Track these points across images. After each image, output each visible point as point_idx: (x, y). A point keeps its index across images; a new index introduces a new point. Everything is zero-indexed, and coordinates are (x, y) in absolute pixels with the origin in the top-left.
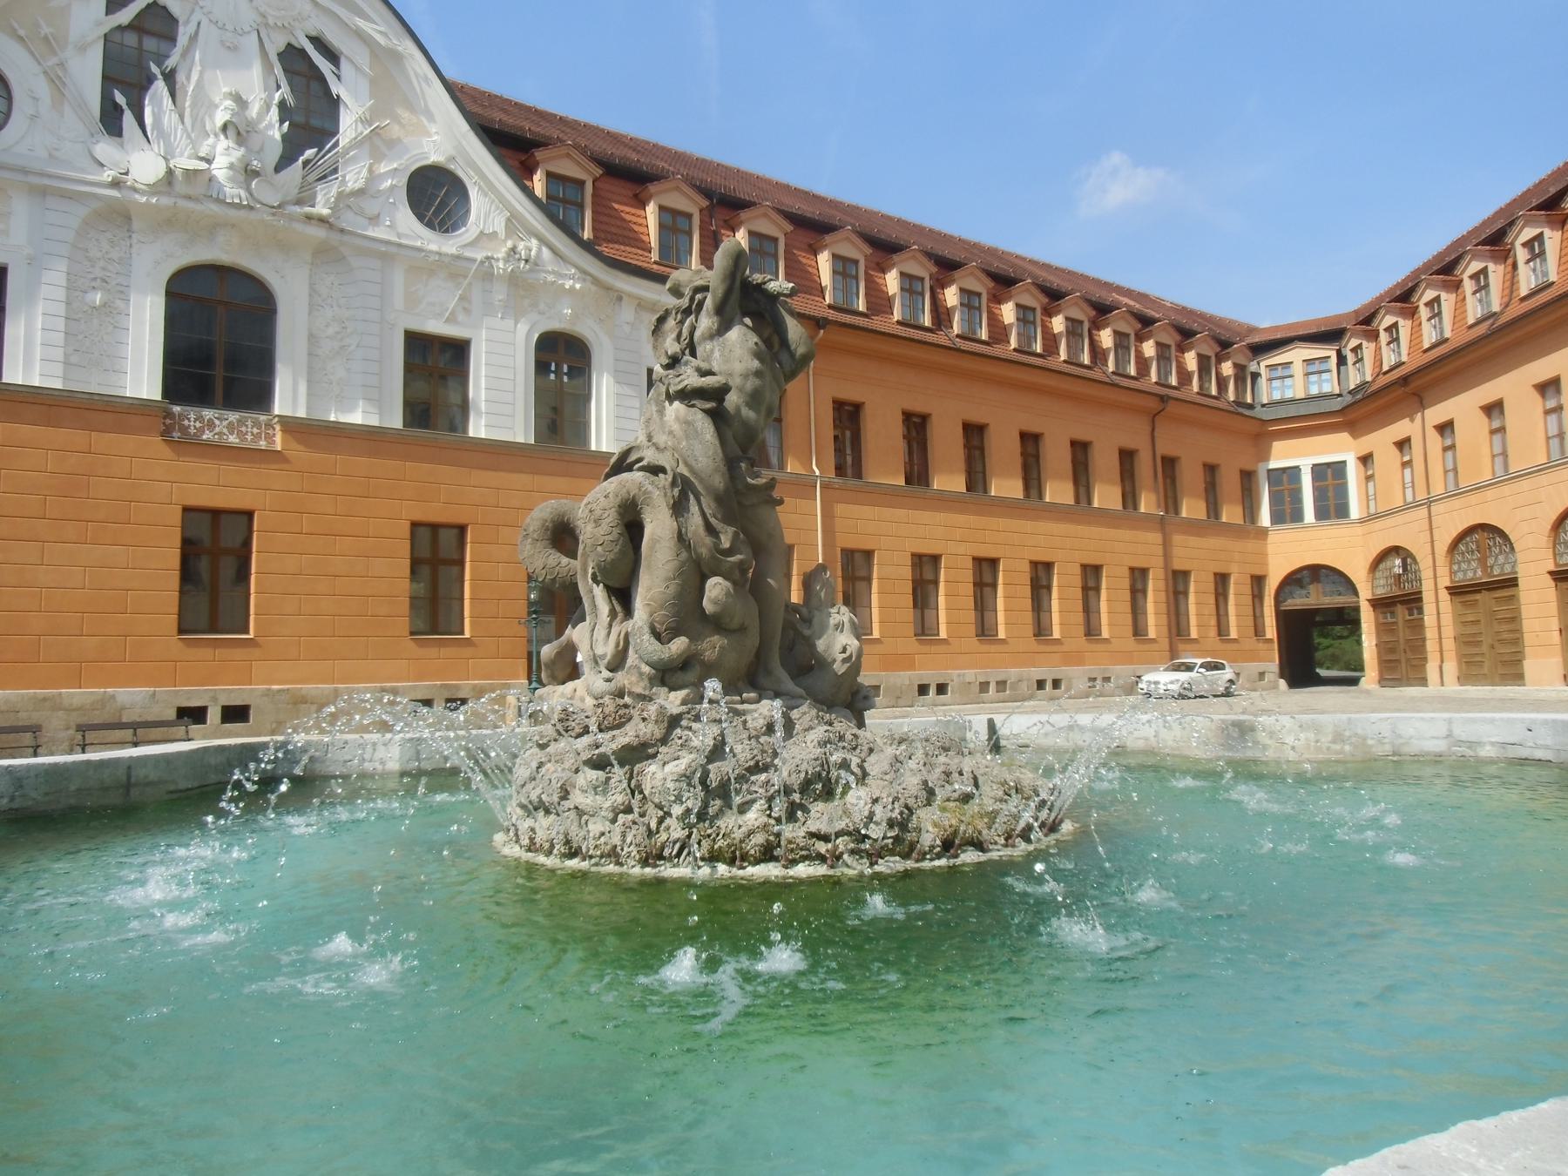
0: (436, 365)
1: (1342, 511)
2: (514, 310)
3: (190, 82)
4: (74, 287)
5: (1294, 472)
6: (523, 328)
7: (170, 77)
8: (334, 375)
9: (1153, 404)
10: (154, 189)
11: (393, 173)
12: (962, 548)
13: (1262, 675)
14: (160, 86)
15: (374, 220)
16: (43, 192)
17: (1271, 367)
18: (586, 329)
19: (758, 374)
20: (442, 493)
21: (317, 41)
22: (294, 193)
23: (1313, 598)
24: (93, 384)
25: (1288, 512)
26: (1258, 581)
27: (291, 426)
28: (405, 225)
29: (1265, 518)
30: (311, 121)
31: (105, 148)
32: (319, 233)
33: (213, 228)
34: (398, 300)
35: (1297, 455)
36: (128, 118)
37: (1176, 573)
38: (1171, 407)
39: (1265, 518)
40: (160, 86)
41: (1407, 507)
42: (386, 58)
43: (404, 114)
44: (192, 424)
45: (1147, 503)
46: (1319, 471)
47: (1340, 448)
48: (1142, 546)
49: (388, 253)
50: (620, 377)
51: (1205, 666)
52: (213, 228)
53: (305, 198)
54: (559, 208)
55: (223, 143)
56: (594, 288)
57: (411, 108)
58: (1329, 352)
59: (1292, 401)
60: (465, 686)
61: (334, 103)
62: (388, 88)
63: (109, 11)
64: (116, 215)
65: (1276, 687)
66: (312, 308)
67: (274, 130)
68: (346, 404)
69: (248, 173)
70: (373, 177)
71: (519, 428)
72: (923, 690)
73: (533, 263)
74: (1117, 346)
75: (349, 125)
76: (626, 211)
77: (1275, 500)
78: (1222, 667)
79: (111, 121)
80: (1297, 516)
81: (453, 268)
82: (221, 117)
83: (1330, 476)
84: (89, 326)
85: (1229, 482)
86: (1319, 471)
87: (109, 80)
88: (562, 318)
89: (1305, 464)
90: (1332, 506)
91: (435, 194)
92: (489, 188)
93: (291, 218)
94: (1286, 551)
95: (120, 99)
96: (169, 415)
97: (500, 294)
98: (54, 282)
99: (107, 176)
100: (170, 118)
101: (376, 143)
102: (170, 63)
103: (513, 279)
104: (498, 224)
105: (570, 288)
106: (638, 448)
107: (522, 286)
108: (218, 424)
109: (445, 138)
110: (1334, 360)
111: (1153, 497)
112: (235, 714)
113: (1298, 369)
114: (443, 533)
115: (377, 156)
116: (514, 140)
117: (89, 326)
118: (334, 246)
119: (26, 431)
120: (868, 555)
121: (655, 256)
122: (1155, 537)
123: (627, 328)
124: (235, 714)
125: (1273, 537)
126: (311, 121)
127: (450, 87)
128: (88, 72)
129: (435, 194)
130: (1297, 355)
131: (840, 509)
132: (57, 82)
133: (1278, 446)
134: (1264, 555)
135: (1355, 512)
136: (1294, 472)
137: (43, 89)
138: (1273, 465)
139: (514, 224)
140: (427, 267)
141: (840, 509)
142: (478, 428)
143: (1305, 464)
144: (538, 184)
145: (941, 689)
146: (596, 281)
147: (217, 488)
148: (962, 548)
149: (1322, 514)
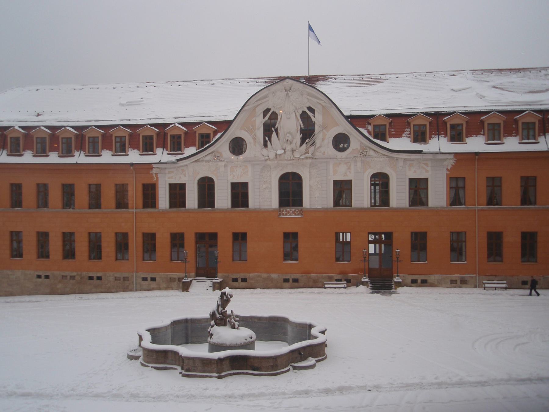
0: (342, 189)
7: (276, 130)
14: (274, 134)
18: (387, 170)
19: (209, 332)
21: (310, 109)
22: (304, 151)
32: (309, 161)
34: (331, 173)
36: (269, 142)
40: (274, 134)
41: (178, 253)
56: (387, 159)
61: (314, 124)
63: (264, 118)
79: (265, 145)
87: (265, 135)
93: (303, 159)
95: (267, 138)
96: (280, 211)
102: (276, 126)
106: (141, 362)
108: (291, 213)
112: (39, 277)
114: (91, 186)
123: (401, 168)
124: (39, 277)
128: (260, 133)
132: (254, 138)
137: (252, 140)
146: (388, 156)
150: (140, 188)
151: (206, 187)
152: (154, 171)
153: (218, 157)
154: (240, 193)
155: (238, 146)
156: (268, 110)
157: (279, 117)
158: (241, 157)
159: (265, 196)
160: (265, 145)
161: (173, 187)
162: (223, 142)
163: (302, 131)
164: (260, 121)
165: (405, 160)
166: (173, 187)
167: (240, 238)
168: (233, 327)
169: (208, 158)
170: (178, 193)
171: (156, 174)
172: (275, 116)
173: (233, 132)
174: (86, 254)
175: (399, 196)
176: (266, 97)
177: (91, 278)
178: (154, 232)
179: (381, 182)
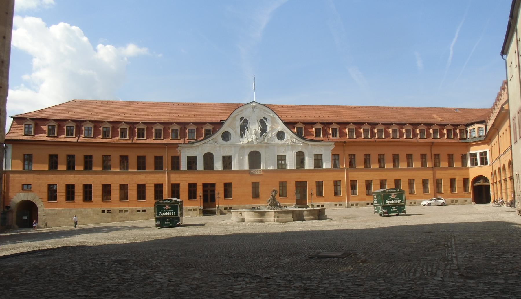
0: (282, 159)
1: (486, 163)
2: (292, 150)
3: (250, 129)
4: (239, 157)
5: (475, 154)
6: (294, 152)
8: (268, 164)
9: (431, 144)
10: (247, 144)
11: (274, 133)
12: (377, 178)
13: (466, 201)
15: (272, 141)
16: (235, 146)
17: (470, 130)
20: (283, 177)
21: (264, 118)
23: (482, 183)
24: (241, 169)
25: (474, 163)
26: (465, 181)
27: (263, 171)
28: (277, 141)
29: (469, 164)
30: (264, 130)
31: (241, 139)
32: (265, 145)
33: (253, 147)
35: (477, 150)
37: (437, 180)
38: (434, 144)
39: (469, 164)
42: (273, 118)
43: (275, 124)
44: (252, 172)
45: (429, 165)
46: (481, 154)
47: (485, 148)
48: (428, 175)
49: (274, 145)
50: (309, 157)
51: (435, 200)
52: (253, 147)
53: (264, 140)
54: (299, 134)
55: (254, 136)
57: (277, 123)
58: (483, 126)
59: (475, 137)
60: (287, 204)
61: (267, 126)
62: (273, 122)
64: (243, 147)
65: (471, 204)
66: (265, 154)
67: (259, 132)
68: (270, 166)
69: (257, 139)
70: (272, 135)
71: (294, 167)
72: (368, 204)
73: (295, 143)
74: (420, 133)
75: (269, 128)
76: (309, 130)
77: (472, 160)
78: (442, 200)
79: (241, 136)
80: (476, 164)
81: (283, 145)
82: (253, 133)
83: (484, 155)
84: (241, 162)
85: (457, 156)
86: (481, 154)
88: (300, 149)
89: (478, 152)
90: (484, 161)
91: (280, 135)
92: (287, 133)
94: (474, 172)
97: (290, 148)
98: (237, 155)
99: (242, 143)
100: (248, 134)
101: (272, 130)
103: (292, 145)
104: (289, 138)
105: (300, 144)
107: (293, 146)
108: (255, 172)
109: (281, 127)
110: (484, 128)
111: (430, 163)
112: (103, 211)
113: (476, 130)
115: (272, 132)
116: (290, 125)
117: (241, 162)
118: (267, 146)
119: (235, 175)
120: (452, 155)
121: (315, 136)
122: (431, 172)
124: (103, 211)
125: (470, 169)
126: (264, 130)
127: (282, 121)
129: (280, 135)
130: (476, 127)
131: (350, 173)
132: (236, 132)
133: (472, 148)
134: (468, 174)
135: (489, 163)
136: (475, 154)
137: (234, 134)
138: (471, 152)
139: (292, 137)
140: (279, 146)
141: (350, 173)
142: (288, 168)
143: (478, 152)
144: (295, 129)
145: (415, 203)
147: (255, 180)
148: (377, 178)
149: (482, 163)
150: (170, 158)
151: (209, 158)
152: (179, 148)
153: (216, 142)
154: (227, 161)
155: (226, 136)
156: (242, 118)
157: (249, 122)
158: (229, 142)
159: (241, 163)
160: (241, 136)
161: (189, 158)
162: (464, 216)
163: (261, 129)
164: (238, 124)
165: (312, 145)
166: (189, 158)
167: (227, 187)
168: (222, 213)
169: (210, 142)
170: (192, 162)
171: (180, 151)
172: (246, 121)
173: (224, 128)
174: (136, 197)
175: (309, 164)
176: (242, 111)
177: (139, 211)
178: (178, 183)
179: (300, 157)
